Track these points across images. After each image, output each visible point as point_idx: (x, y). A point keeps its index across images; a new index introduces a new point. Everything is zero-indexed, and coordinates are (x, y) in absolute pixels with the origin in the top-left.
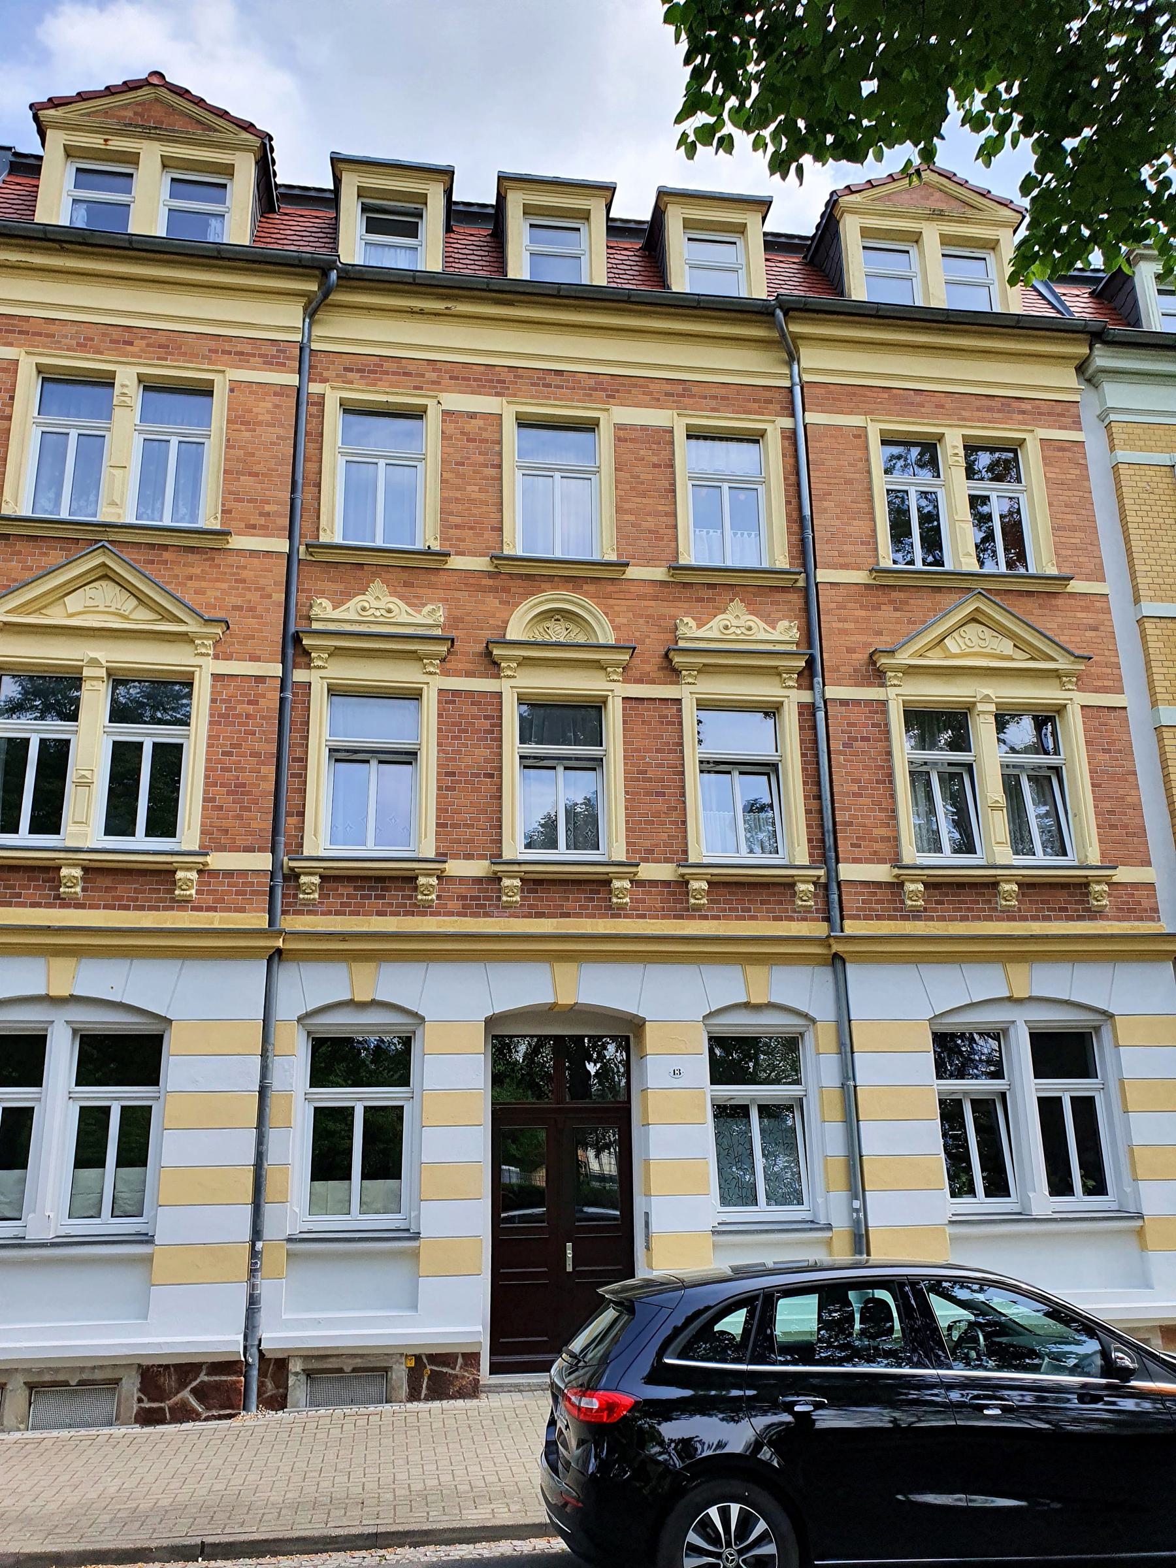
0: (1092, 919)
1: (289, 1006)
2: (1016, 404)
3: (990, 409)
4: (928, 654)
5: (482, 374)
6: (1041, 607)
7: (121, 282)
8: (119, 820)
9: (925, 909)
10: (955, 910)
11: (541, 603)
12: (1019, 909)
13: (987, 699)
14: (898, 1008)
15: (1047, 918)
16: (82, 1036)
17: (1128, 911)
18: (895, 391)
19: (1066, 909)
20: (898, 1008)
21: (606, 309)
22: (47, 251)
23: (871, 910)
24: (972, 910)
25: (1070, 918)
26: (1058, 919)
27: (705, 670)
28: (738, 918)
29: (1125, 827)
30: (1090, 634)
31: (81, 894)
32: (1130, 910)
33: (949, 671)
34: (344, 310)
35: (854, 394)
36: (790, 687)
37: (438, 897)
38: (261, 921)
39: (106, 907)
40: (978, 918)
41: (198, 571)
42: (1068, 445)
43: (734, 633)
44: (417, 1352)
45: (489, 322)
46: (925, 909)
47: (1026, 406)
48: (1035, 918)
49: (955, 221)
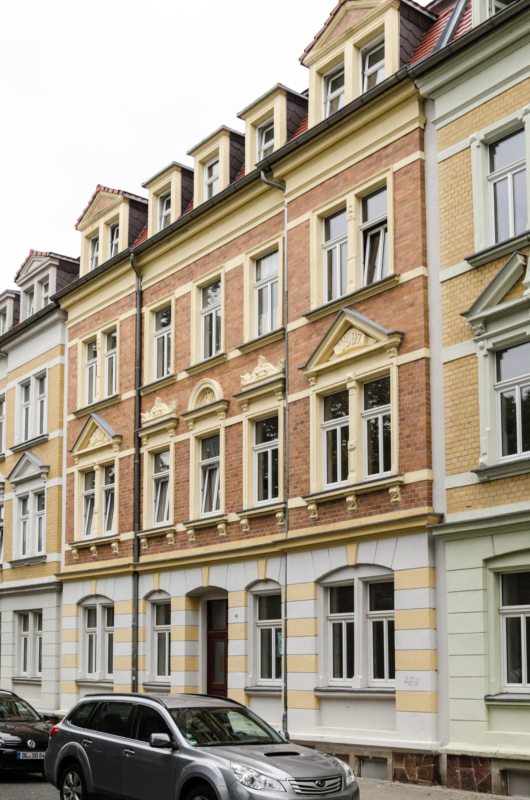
0: (392, 510)
1: (143, 593)
2: (383, 153)
3: (370, 165)
4: (330, 359)
5: (187, 271)
6: (385, 301)
7: (201, 233)
8: (374, 468)
9: (319, 519)
10: (332, 516)
11: (199, 388)
12: (358, 511)
13: (350, 380)
14: (300, 578)
15: (371, 514)
16: (370, 585)
17: (410, 503)
18: (325, 183)
19: (379, 507)
20: (300, 578)
21: (246, 190)
22: (177, 235)
23: (299, 523)
24: (337, 516)
25: (381, 512)
26: (376, 513)
27: (196, 421)
28: (260, 536)
29: (415, 444)
30: (409, 310)
31: (97, 556)
32: (412, 501)
33: (336, 367)
34: (149, 264)
35: (308, 198)
36: (116, 451)
37: (175, 542)
38: (129, 560)
39: (103, 560)
40: (340, 520)
41: (115, 415)
42: (410, 167)
43: (262, 375)
44: (412, 752)
45: (94, 293)
46: (319, 519)
47: (390, 150)
48: (365, 515)
49: (361, 28)
